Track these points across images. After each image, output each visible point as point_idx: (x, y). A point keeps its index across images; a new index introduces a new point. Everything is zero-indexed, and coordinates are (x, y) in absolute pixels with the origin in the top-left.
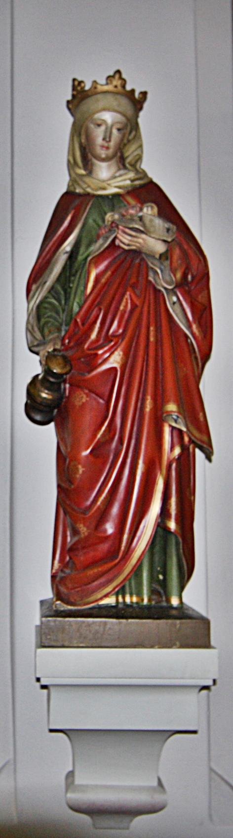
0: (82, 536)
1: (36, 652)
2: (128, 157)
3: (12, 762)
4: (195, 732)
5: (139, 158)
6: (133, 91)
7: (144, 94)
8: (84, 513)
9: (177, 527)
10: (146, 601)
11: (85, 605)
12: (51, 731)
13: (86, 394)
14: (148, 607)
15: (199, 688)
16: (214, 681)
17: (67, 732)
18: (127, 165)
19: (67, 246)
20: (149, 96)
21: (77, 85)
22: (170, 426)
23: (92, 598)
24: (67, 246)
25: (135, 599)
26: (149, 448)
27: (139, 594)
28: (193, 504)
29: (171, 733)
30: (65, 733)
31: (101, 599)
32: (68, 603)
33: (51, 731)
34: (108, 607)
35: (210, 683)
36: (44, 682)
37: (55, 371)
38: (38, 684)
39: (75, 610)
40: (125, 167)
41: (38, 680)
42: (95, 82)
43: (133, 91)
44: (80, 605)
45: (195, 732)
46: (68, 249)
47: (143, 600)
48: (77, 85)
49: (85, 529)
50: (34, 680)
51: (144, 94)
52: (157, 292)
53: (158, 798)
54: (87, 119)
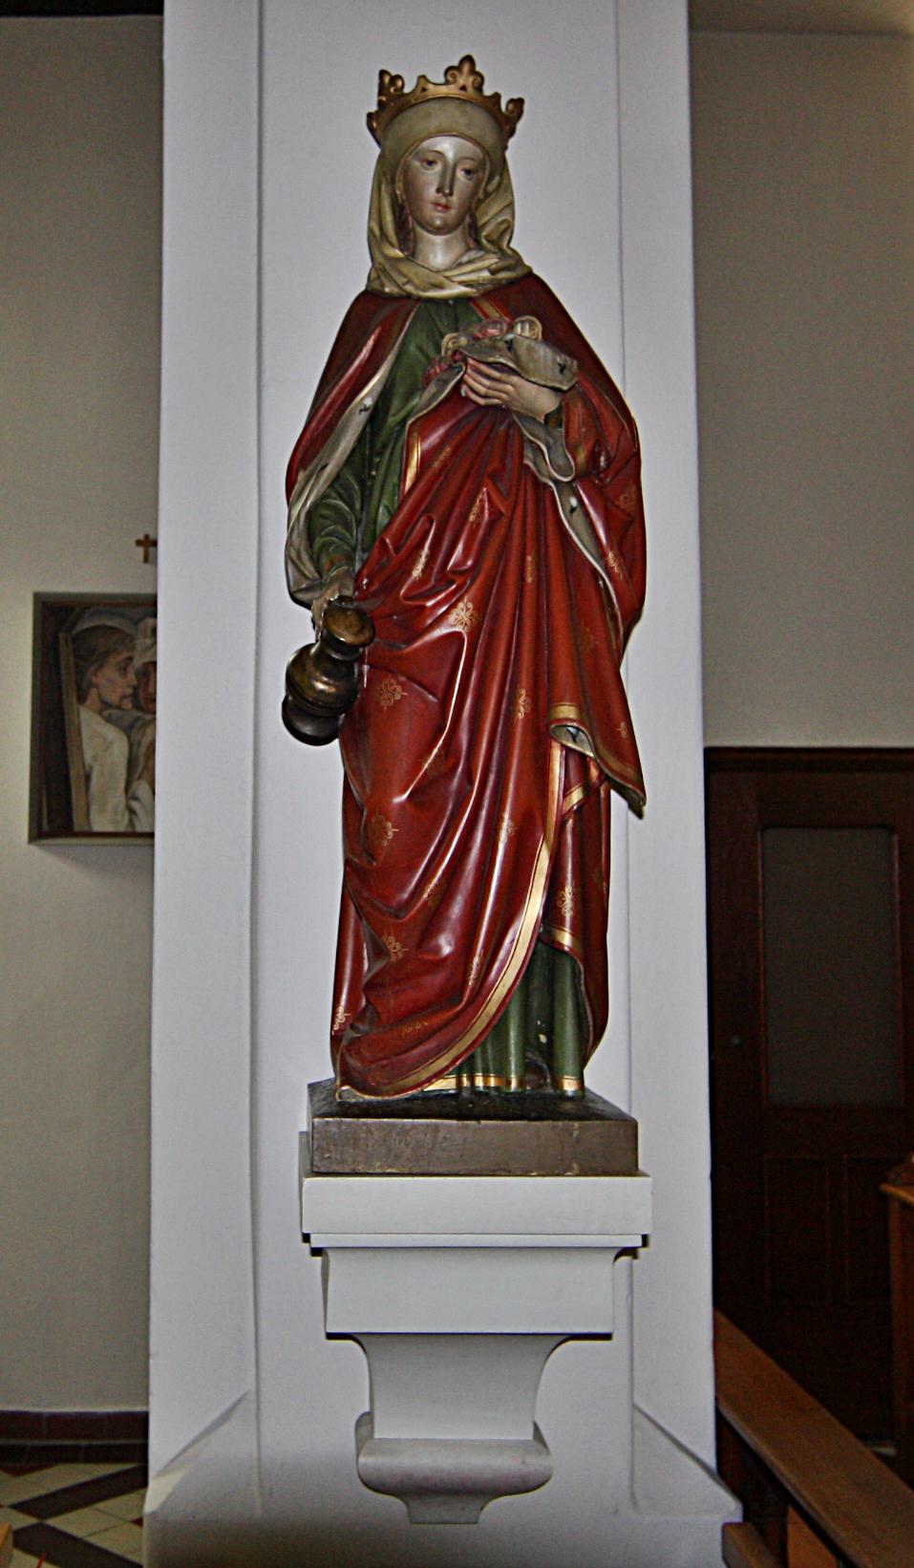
4: (607, 1337)
5: (508, 229)
6: (497, 97)
7: (518, 104)
12: (331, 1336)
16: (645, 1239)
17: (361, 1339)
21: (388, 83)
22: (564, 747)
23: (412, 1080)
27: (502, 1073)
31: (429, 1081)
33: (331, 1336)
34: (442, 1096)
39: (378, 1102)
40: (479, 246)
41: (306, 1238)
43: (497, 97)
45: (607, 1337)
49: (398, 946)
50: (300, 1238)
51: (518, 104)
53: (534, 1463)
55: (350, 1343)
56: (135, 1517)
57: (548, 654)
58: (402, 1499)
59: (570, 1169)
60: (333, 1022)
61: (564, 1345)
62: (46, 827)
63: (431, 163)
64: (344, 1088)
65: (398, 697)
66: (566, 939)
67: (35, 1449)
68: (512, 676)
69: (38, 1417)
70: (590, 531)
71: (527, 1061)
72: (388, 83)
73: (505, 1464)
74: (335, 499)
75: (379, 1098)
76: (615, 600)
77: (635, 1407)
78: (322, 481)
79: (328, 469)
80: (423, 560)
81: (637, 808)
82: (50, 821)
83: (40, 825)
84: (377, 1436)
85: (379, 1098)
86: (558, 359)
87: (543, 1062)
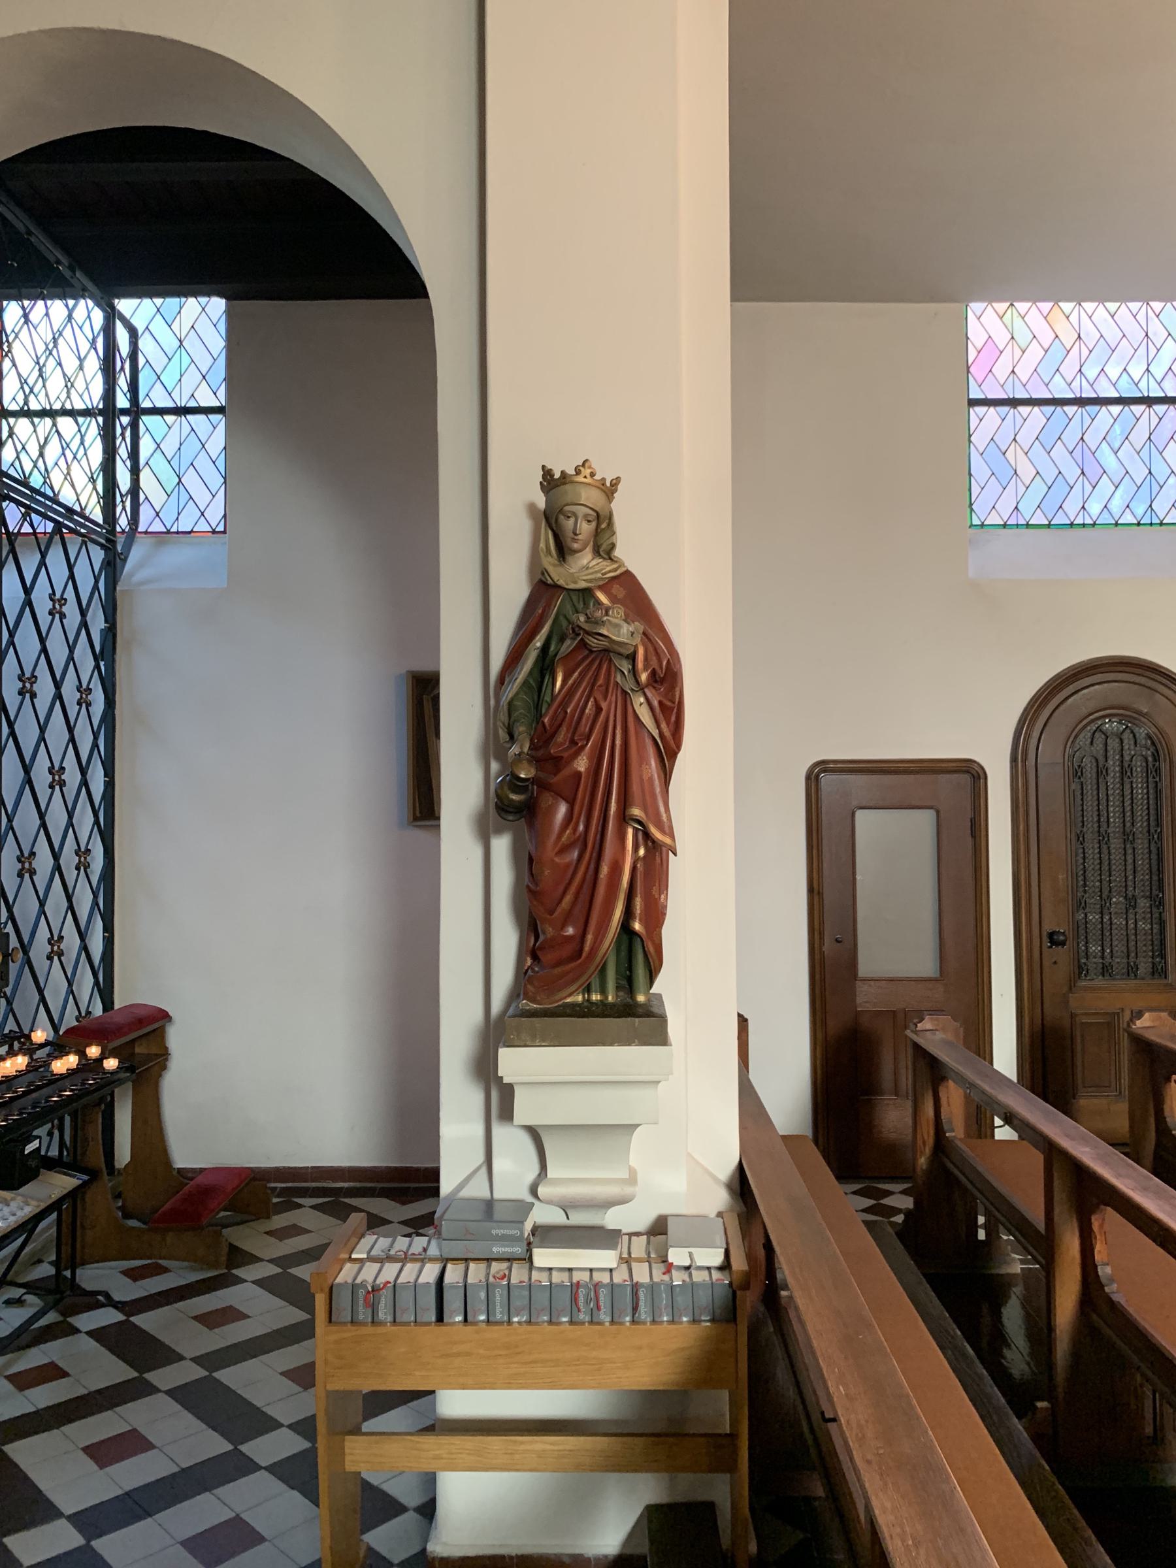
0: (549, 936)
2: (602, 544)
5: (613, 546)
6: (604, 479)
8: (551, 912)
9: (631, 924)
10: (610, 998)
11: (557, 1001)
13: (552, 797)
14: (613, 1005)
18: (602, 553)
19: (538, 643)
21: (547, 473)
22: (634, 828)
23: (557, 998)
24: (538, 640)
25: (599, 997)
27: (603, 992)
28: (102, 877)
31: (565, 998)
32: (534, 1001)
34: (574, 1005)
37: (522, 776)
39: (540, 1008)
40: (599, 555)
42: (562, 472)
43: (604, 479)
44: (545, 1004)
46: (539, 644)
47: (607, 998)
49: (551, 929)
51: (616, 483)
52: (625, 693)
53: (628, 1190)
54: (91, 1122)
59: (634, 1042)
60: (667, 894)
62: (418, 814)
63: (569, 517)
64: (524, 1001)
65: (550, 803)
66: (637, 926)
67: (416, 1189)
69: (418, 1170)
72: (547, 473)
73: (613, 1191)
75: (541, 1006)
76: (663, 751)
78: (515, 686)
79: (518, 681)
80: (576, 718)
81: (675, 854)
82: (420, 812)
83: (414, 814)
84: (549, 1176)
85: (541, 1006)
86: (630, 629)
87: (628, 983)
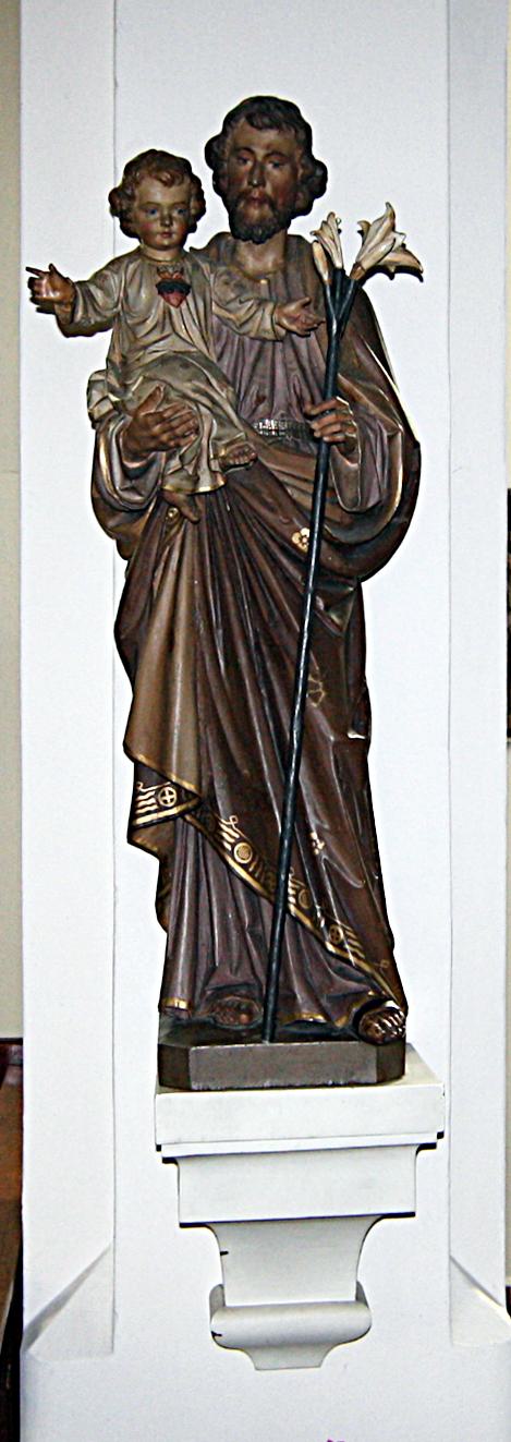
1: (235, 1309)
3: (112, 1250)
4: (412, 1215)
7: (51, 266)
12: (183, 1225)
15: (416, 1148)
16: (440, 1135)
17: (211, 1226)
20: (55, 265)
21: (359, 232)
26: (134, 598)
29: (374, 1219)
30: (209, 1227)
33: (183, 1225)
35: (432, 1139)
36: (167, 1152)
38: (159, 1156)
41: (159, 1148)
45: (412, 1215)
48: (359, 232)
50: (155, 1148)
51: (51, 266)
53: (352, 1319)
55: (204, 1230)
56: (224, 1257)
57: (259, 690)
58: (247, 1354)
61: (378, 1224)
68: (302, 641)
70: (160, 688)
71: (376, 964)
74: (215, 352)
77: (452, 1259)
